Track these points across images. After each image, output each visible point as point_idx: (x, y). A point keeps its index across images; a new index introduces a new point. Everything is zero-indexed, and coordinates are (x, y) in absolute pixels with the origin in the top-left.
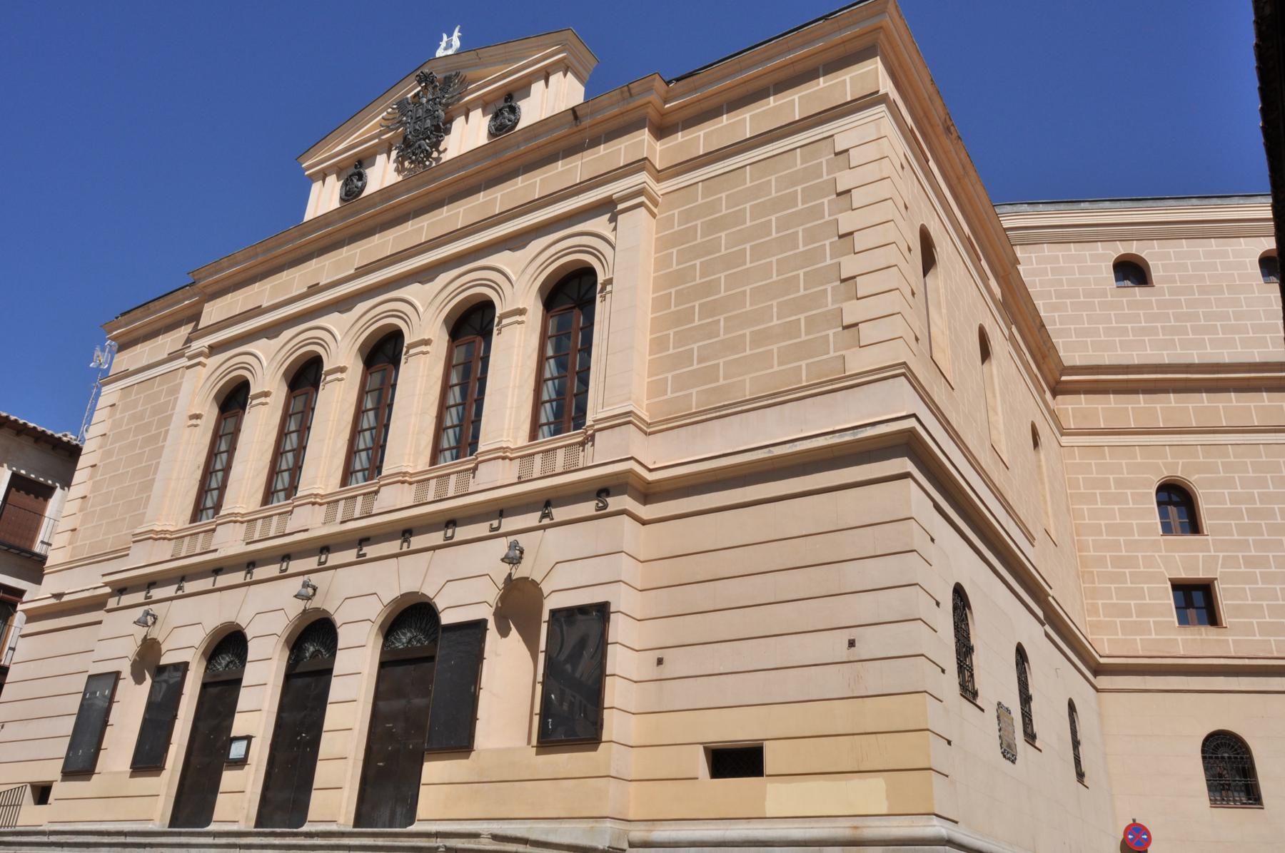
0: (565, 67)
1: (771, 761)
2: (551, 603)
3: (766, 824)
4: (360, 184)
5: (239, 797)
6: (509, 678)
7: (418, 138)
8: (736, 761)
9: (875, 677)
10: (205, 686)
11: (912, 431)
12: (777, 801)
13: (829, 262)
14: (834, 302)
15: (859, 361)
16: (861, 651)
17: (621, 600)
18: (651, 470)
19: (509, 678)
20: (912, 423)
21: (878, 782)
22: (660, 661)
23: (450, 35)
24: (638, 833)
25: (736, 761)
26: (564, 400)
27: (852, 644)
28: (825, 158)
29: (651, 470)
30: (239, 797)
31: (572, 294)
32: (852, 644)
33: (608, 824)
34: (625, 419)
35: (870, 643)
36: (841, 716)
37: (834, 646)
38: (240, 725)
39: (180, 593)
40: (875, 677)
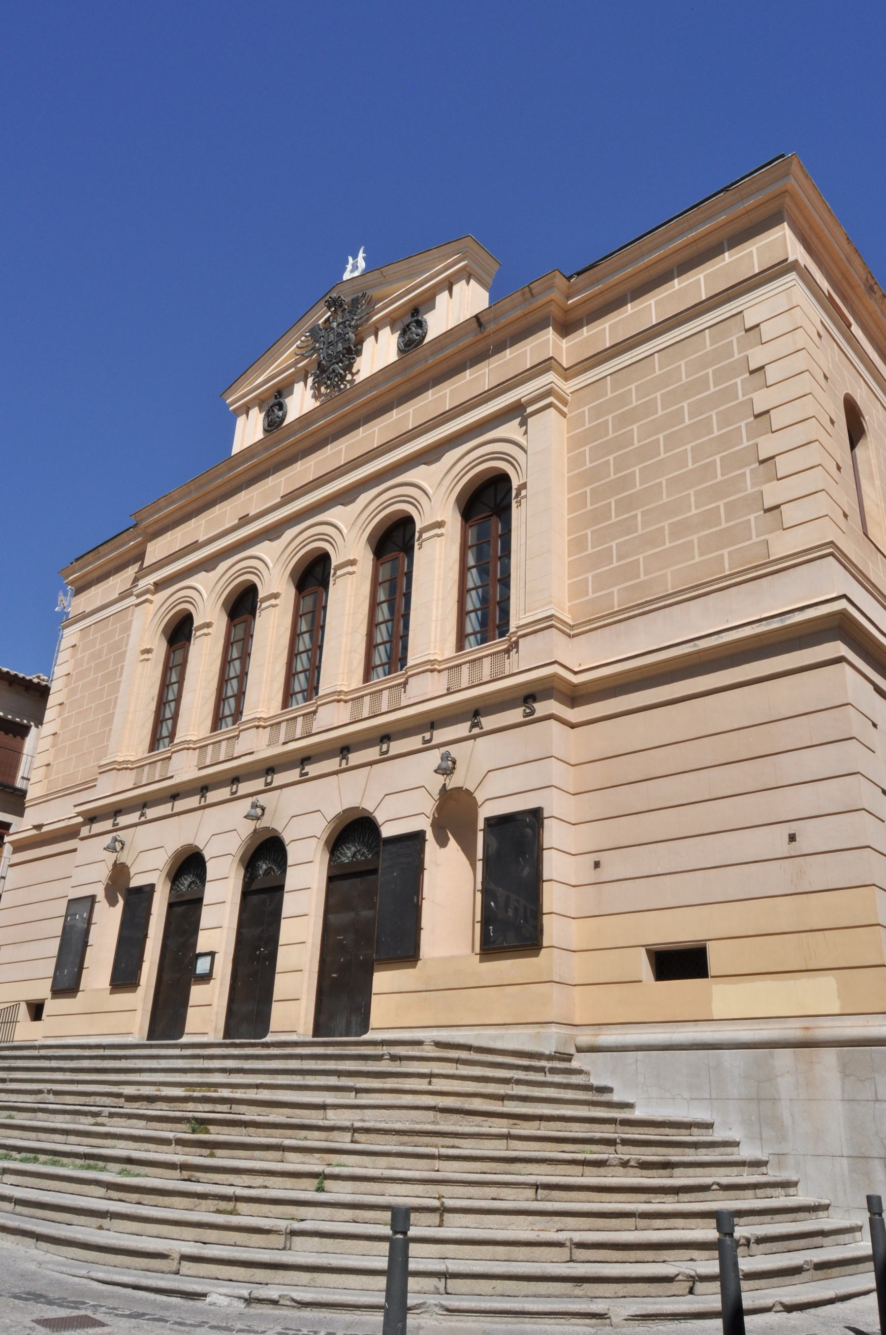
0: (467, 275)
1: (715, 961)
2: (486, 811)
3: (714, 1026)
4: (280, 413)
5: (207, 1008)
6: (450, 886)
7: (331, 363)
8: (680, 963)
9: (818, 873)
10: (171, 906)
11: (843, 613)
12: (723, 1001)
13: (745, 443)
14: (753, 485)
15: (784, 544)
16: (802, 845)
17: (554, 805)
18: (576, 673)
19: (450, 886)
20: (843, 604)
21: (828, 983)
22: (597, 865)
23: (355, 257)
24: (585, 1038)
25: (680, 963)
26: (487, 612)
27: (792, 838)
28: (735, 336)
29: (576, 673)
30: (207, 1008)
31: (488, 502)
32: (792, 838)
33: (554, 1029)
34: (547, 624)
35: (813, 836)
36: (784, 913)
37: (774, 841)
38: (204, 943)
39: (143, 819)
40: (818, 873)
